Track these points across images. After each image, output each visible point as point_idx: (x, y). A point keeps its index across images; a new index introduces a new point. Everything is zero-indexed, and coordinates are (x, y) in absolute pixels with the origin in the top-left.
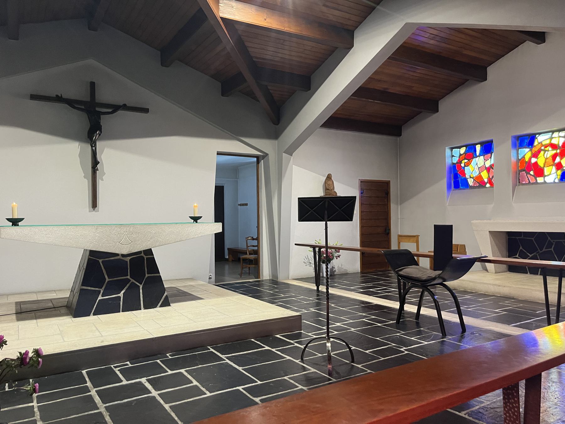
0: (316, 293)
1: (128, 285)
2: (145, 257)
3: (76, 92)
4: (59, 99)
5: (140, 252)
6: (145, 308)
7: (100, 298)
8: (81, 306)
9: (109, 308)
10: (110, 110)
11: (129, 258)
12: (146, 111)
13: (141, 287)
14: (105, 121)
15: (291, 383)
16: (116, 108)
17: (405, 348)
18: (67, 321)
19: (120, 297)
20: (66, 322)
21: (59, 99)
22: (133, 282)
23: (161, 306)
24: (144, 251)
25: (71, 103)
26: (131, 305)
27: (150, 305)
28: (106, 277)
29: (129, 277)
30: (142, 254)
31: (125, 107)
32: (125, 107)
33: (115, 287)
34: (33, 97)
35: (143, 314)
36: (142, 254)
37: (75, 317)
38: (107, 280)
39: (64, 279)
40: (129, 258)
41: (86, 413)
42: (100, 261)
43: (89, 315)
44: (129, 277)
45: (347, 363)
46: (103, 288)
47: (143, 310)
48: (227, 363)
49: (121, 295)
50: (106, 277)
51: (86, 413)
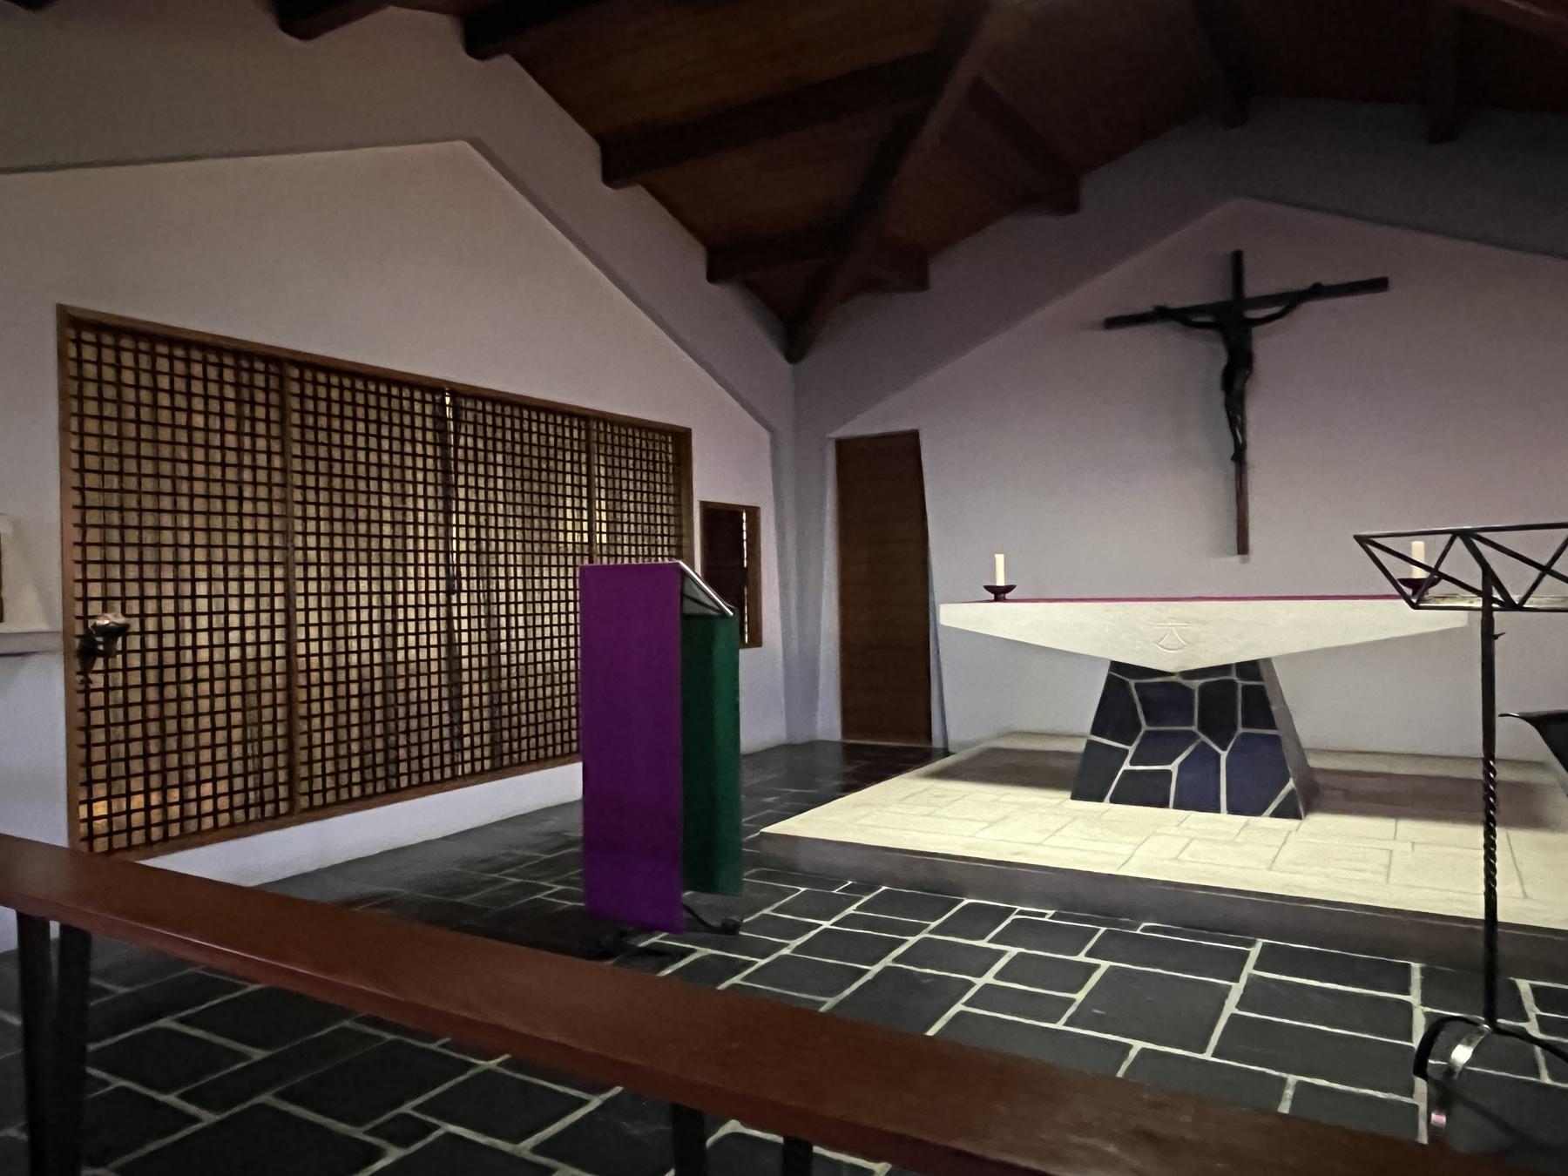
0: (1479, 793)
1: (1191, 748)
2: (1240, 683)
3: (1197, 287)
4: (1162, 314)
5: (1225, 669)
6: (1233, 810)
7: (1126, 766)
8: (1087, 779)
9: (1144, 792)
11: (1196, 684)
13: (1224, 755)
14: (1268, 346)
16: (1290, 301)
18: (1058, 802)
19: (1169, 773)
21: (1162, 314)
22: (1204, 744)
23: (1277, 814)
24: (1239, 665)
25: (1181, 317)
26: (1198, 798)
27: (1245, 805)
28: (1142, 718)
29: (1194, 728)
30: (1234, 677)
31: (1317, 291)
32: (1317, 291)
34: (1112, 323)
35: (1224, 822)
36: (1234, 677)
38: (1145, 727)
39: (1073, 716)
40: (1196, 684)
42: (1132, 683)
44: (1194, 728)
45: (1118, 1068)
47: (1224, 816)
48: (982, 938)
49: (1174, 767)
50: (1142, 718)
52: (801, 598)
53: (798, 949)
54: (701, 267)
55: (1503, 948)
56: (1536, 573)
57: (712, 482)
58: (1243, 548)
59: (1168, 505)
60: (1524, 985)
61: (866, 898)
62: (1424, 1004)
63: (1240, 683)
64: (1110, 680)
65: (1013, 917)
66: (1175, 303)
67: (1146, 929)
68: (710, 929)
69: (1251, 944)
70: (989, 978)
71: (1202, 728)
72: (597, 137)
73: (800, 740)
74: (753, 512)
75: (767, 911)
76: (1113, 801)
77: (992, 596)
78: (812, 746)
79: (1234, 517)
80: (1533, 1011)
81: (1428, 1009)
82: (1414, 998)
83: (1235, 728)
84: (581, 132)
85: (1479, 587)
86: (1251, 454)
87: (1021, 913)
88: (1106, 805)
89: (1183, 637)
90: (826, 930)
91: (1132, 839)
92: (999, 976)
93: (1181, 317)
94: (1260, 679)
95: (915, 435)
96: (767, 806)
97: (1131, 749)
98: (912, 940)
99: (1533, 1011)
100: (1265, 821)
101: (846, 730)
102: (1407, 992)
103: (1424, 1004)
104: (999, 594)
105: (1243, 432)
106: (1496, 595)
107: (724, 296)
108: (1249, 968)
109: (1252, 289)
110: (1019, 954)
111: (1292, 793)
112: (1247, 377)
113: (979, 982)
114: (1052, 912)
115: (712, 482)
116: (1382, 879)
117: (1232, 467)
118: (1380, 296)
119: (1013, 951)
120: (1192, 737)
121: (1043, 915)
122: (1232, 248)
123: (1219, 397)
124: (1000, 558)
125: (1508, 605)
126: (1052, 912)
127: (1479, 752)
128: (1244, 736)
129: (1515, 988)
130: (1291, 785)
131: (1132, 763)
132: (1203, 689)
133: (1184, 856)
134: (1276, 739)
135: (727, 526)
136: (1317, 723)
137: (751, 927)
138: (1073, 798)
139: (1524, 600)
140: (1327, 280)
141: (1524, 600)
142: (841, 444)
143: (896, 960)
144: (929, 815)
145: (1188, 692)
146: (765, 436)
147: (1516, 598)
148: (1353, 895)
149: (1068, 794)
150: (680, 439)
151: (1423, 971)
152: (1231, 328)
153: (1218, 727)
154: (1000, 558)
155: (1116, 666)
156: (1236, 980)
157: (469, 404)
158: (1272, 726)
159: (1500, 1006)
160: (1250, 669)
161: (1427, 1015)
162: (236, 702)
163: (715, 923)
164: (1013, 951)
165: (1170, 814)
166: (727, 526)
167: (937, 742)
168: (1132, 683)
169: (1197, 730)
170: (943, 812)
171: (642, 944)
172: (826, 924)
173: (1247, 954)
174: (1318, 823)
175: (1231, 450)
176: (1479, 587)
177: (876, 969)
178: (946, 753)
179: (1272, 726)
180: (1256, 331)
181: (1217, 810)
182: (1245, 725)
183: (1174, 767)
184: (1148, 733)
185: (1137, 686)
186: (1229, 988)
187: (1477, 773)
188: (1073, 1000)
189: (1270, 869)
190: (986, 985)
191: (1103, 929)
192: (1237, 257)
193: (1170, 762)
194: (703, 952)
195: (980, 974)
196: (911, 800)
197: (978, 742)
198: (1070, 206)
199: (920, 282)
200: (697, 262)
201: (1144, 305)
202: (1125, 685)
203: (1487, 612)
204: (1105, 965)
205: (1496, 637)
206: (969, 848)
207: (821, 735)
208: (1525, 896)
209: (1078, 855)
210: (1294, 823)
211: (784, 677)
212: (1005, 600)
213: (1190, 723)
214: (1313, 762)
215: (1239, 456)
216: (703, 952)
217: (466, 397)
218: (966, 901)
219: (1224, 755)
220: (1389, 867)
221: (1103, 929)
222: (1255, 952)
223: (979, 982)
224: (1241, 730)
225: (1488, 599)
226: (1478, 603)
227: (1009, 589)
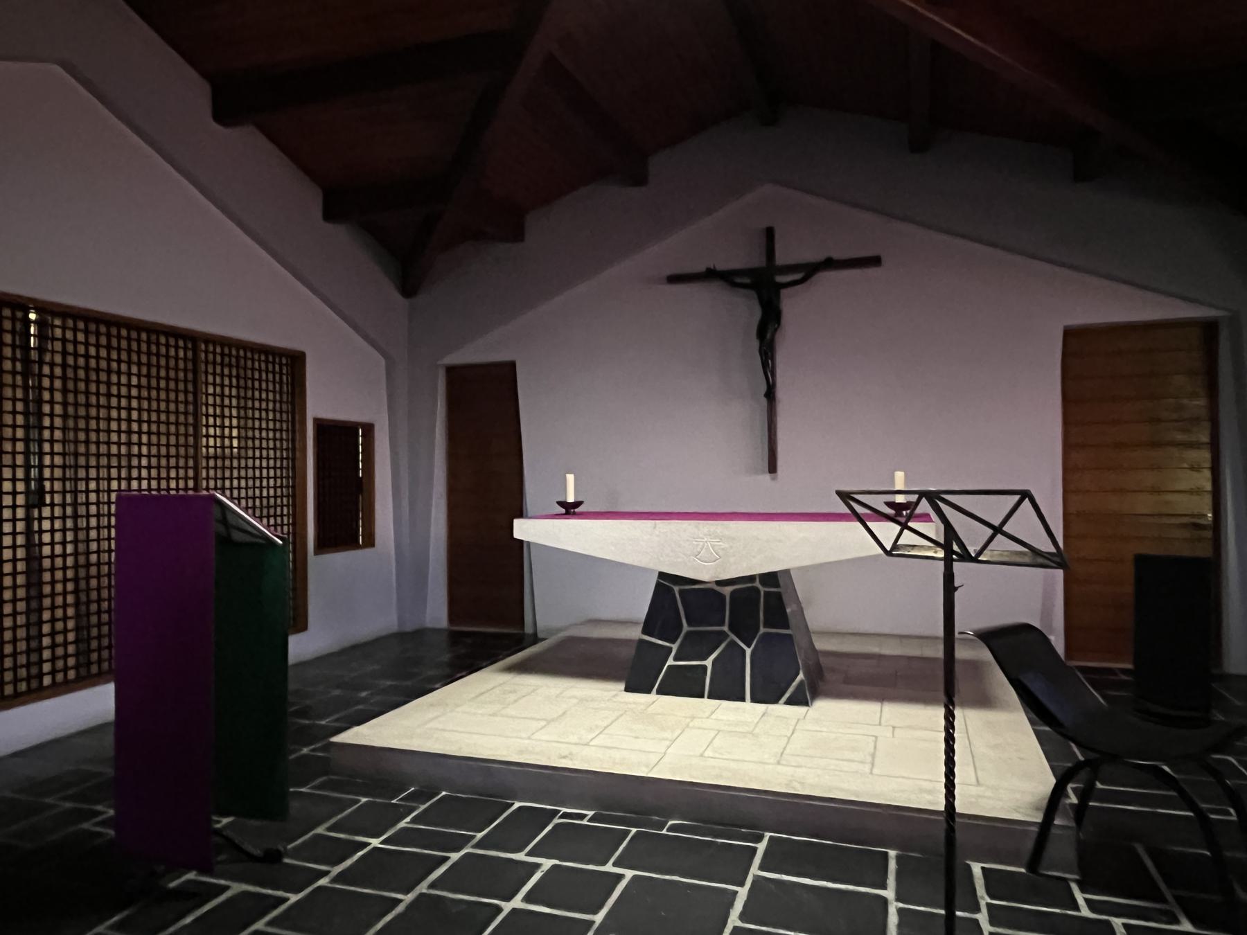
2: (762, 590)
3: (739, 255)
4: (710, 275)
5: (751, 578)
7: (670, 662)
8: (639, 673)
10: (798, 276)
11: (727, 591)
12: (875, 261)
13: (748, 651)
14: (793, 305)
15: (365, 888)
16: (810, 271)
17: (323, 882)
18: (610, 694)
20: (605, 698)
21: (710, 275)
23: (789, 702)
25: (727, 278)
27: (766, 695)
28: (684, 621)
29: (726, 628)
30: (757, 584)
31: (830, 264)
32: (830, 264)
33: (697, 646)
34: (674, 279)
35: (745, 713)
36: (757, 584)
37: (628, 689)
38: (686, 628)
40: (727, 591)
41: (591, 867)
42: (676, 589)
43: (649, 691)
44: (726, 628)
46: (679, 641)
47: (748, 705)
48: (518, 850)
49: (708, 663)
50: (684, 621)
51: (591, 867)
52: (412, 504)
53: (339, 878)
54: (317, 212)
55: (959, 836)
56: (990, 532)
57: (323, 403)
58: (772, 468)
59: (703, 435)
60: (976, 868)
61: (423, 807)
62: (898, 899)
63: (762, 590)
64: (658, 586)
65: (556, 821)
66: (721, 266)
67: (672, 829)
68: (252, 858)
69: (759, 839)
70: (517, 902)
71: (731, 628)
72: (204, 75)
73: (409, 628)
74: (369, 429)
75: (320, 830)
76: (659, 692)
77: (563, 511)
78: (419, 635)
79: (775, 434)
80: (984, 899)
81: (901, 905)
82: (889, 893)
83: (758, 629)
84: (192, 74)
85: (942, 541)
86: (781, 393)
87: (565, 815)
88: (653, 696)
89: (717, 552)
90: (375, 849)
91: (667, 735)
92: (527, 899)
93: (727, 278)
94: (778, 586)
95: (513, 365)
96: (363, 701)
97: (675, 647)
98: (455, 856)
99: (984, 899)
100: (780, 710)
101: (452, 617)
102: (884, 887)
103: (898, 899)
104: (570, 510)
105: (773, 375)
106: (955, 548)
107: (340, 234)
108: (754, 870)
109: (781, 259)
110: (554, 866)
111: (801, 682)
112: (776, 330)
113: (507, 907)
114: (591, 813)
115: (323, 403)
116: (867, 768)
117: (764, 401)
118: (871, 272)
119: (547, 863)
120: (723, 635)
121: (582, 817)
122: (769, 225)
123: (756, 344)
124: (570, 478)
125: (966, 557)
126: (591, 813)
127: (940, 631)
128: (765, 634)
129: (969, 868)
130: (801, 676)
131: (676, 659)
132: (733, 593)
133: (709, 753)
134: (790, 636)
135: (343, 446)
136: (827, 617)
137: (296, 853)
138: (627, 689)
139: (980, 553)
140: (836, 255)
141: (980, 553)
142: (451, 370)
143: (433, 886)
144: (494, 715)
145: (721, 597)
146: (383, 362)
147: (972, 550)
148: (842, 790)
149: (622, 686)
150: (296, 361)
151: (898, 858)
152: (765, 289)
153: (745, 629)
154: (570, 478)
155: (662, 575)
156: (742, 884)
157: (57, 322)
158: (787, 626)
159: (959, 899)
160: (770, 578)
161: (900, 911)
162: (70, 548)
163: (257, 852)
164: (547, 863)
165: (706, 703)
166: (343, 446)
167: (528, 629)
168: (676, 589)
169: (727, 635)
170: (511, 711)
171: (173, 885)
172: (375, 842)
173: (755, 850)
174: (823, 708)
175: (764, 388)
176: (942, 541)
177: (409, 898)
178: (535, 639)
179: (787, 626)
180: (784, 292)
181: (743, 700)
182: (765, 626)
183: (708, 663)
184: (689, 634)
185: (681, 592)
186: (736, 892)
187: (938, 652)
188: (593, 922)
189: (779, 763)
190: (514, 910)
191: (634, 830)
192: (770, 233)
193: (705, 659)
194: (237, 888)
195: (508, 898)
196: (482, 698)
197: (559, 630)
198: (640, 180)
199: (517, 234)
200: (313, 200)
201: (700, 267)
202: (670, 590)
203: (948, 562)
204: (629, 874)
205: (956, 589)
206: (521, 752)
207: (429, 623)
208: (978, 783)
209: (617, 755)
210: (800, 710)
211: (347, 601)
212: (574, 514)
213: (722, 624)
214: (820, 645)
215: (770, 394)
216: (237, 888)
217: (55, 314)
218: (517, 805)
219: (748, 651)
220: (873, 756)
221: (634, 830)
222: (762, 847)
223: (507, 907)
224: (762, 630)
225: (947, 547)
226: (941, 554)
227: (577, 504)
